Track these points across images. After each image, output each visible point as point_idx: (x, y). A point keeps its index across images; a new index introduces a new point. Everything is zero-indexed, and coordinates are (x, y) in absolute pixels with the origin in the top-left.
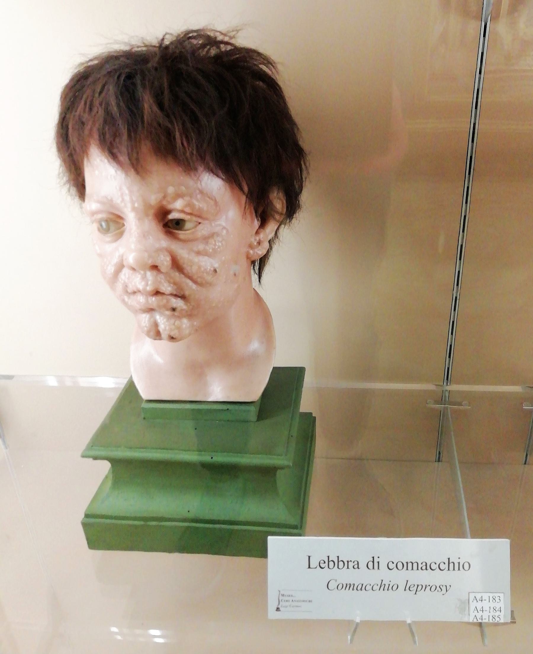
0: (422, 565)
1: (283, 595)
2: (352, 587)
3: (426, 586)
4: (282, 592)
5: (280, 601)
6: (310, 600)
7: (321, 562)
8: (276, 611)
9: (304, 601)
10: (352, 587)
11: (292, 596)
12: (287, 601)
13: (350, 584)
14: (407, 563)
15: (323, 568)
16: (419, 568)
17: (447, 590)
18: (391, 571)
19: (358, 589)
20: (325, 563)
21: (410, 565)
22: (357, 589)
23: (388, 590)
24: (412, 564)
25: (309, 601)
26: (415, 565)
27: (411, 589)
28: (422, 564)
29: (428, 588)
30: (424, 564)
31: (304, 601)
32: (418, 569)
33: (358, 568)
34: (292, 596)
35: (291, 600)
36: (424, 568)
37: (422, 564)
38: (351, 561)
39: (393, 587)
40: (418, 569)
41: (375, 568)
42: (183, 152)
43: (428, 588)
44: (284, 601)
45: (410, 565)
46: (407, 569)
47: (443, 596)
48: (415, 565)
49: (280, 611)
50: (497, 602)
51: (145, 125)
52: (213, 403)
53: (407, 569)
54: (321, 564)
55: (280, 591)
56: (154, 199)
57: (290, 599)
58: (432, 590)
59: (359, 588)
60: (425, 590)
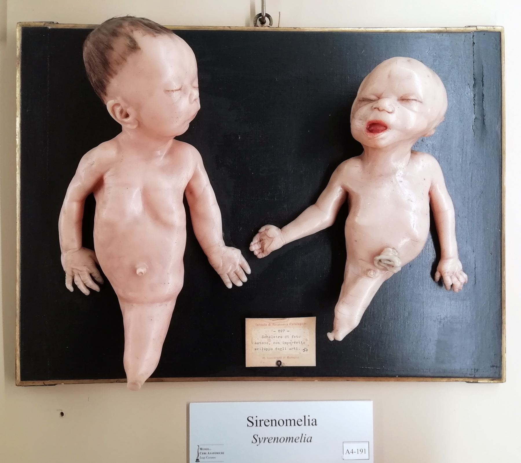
0: (312, 422)
1: (201, 449)
2: (306, 440)
3: (265, 438)
4: (200, 447)
5: (199, 453)
6: (223, 452)
7: (298, 421)
8: (196, 461)
9: (217, 453)
10: (306, 440)
11: (208, 449)
12: (204, 453)
13: (290, 438)
14: (286, 420)
15: (268, 426)
16: (311, 424)
17: (261, 441)
18: (267, 427)
19: (308, 441)
20: (301, 421)
21: (289, 422)
22: (307, 441)
23: (304, 442)
24: (290, 420)
25: (222, 453)
26: (293, 422)
27: (296, 441)
28: (312, 420)
29: (267, 440)
30: (314, 420)
31: (217, 453)
32: (309, 425)
33: (316, 425)
34: (208, 449)
35: (207, 453)
36: (314, 424)
37: (312, 420)
38: (263, 420)
39: (281, 441)
40: (309, 425)
41: (292, 425)
42: (96, 49)
43: (267, 440)
44: (202, 454)
45: (289, 422)
46: (287, 425)
47: (258, 446)
48: (293, 422)
49: (199, 461)
50: (257, 436)
51: (138, 22)
52: (499, 290)
53: (287, 425)
54: (266, 423)
55: (199, 446)
56: (396, 98)
57: (207, 451)
58: (281, 442)
59: (309, 440)
60: (264, 442)
